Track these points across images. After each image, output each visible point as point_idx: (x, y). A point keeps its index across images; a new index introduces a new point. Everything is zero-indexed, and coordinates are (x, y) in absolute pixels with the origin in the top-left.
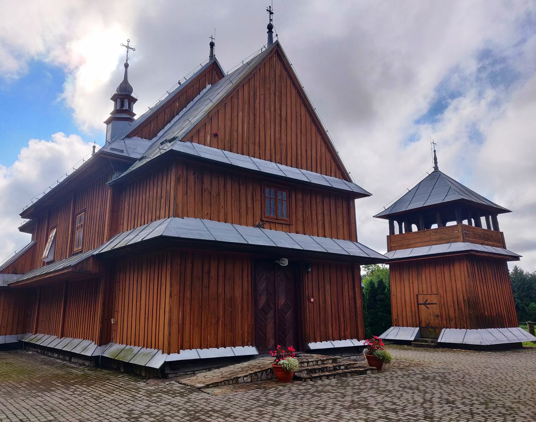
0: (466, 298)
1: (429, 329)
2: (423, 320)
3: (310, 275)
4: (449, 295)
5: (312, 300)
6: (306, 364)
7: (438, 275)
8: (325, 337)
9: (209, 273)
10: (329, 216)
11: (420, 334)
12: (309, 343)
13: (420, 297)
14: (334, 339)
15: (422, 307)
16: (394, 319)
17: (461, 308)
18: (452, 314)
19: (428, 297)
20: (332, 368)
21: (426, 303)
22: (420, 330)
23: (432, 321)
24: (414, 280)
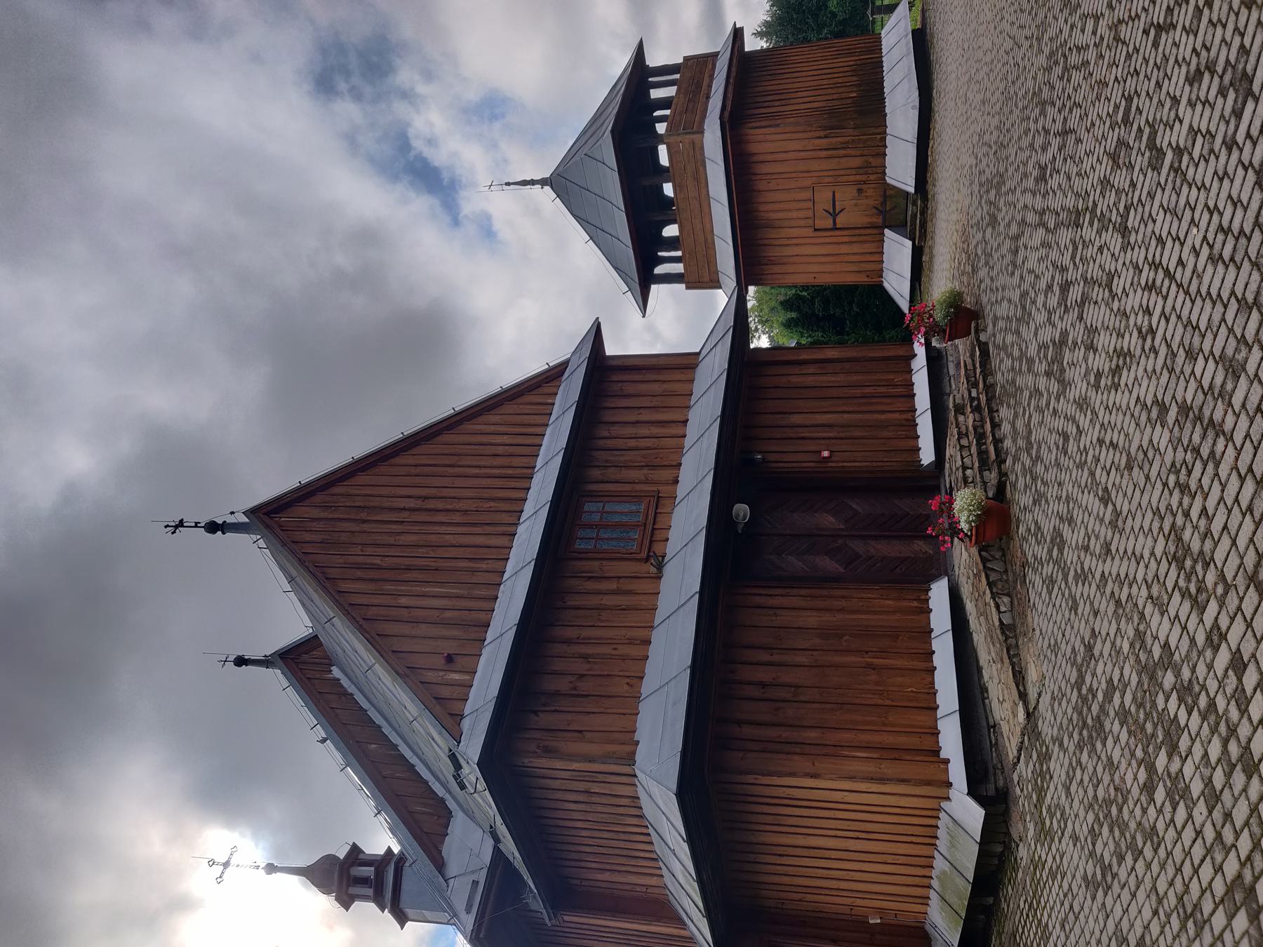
0: (822, 133)
1: (888, 209)
2: (870, 220)
3: (772, 457)
4: (815, 165)
5: (826, 454)
6: (969, 472)
7: (773, 185)
8: (908, 428)
9: (763, 685)
10: (642, 411)
11: (899, 227)
12: (922, 463)
13: (820, 224)
14: (911, 409)
15: (841, 221)
16: (866, 280)
17: (841, 143)
18: (857, 162)
19: (820, 207)
20: (977, 415)
21: (831, 211)
22: (890, 228)
23: (871, 202)
24: (783, 236)
